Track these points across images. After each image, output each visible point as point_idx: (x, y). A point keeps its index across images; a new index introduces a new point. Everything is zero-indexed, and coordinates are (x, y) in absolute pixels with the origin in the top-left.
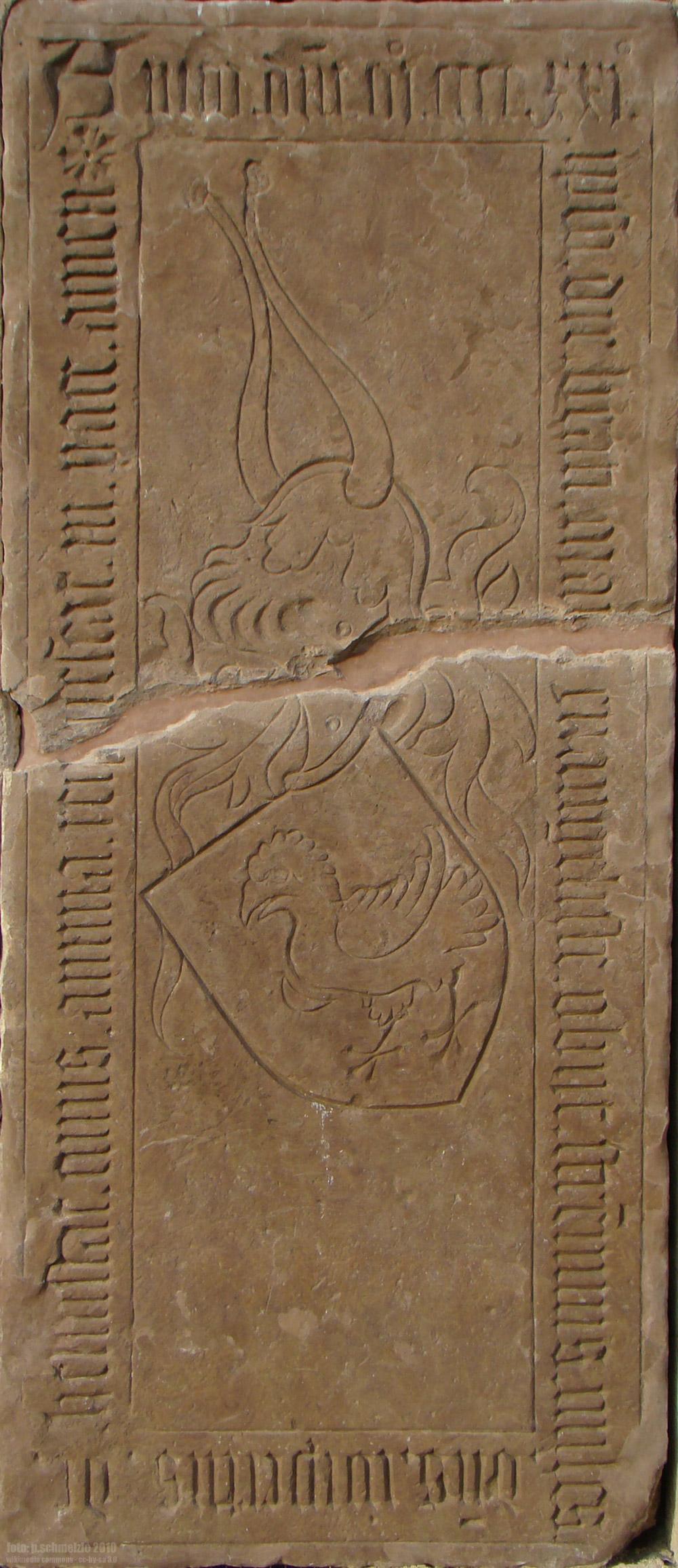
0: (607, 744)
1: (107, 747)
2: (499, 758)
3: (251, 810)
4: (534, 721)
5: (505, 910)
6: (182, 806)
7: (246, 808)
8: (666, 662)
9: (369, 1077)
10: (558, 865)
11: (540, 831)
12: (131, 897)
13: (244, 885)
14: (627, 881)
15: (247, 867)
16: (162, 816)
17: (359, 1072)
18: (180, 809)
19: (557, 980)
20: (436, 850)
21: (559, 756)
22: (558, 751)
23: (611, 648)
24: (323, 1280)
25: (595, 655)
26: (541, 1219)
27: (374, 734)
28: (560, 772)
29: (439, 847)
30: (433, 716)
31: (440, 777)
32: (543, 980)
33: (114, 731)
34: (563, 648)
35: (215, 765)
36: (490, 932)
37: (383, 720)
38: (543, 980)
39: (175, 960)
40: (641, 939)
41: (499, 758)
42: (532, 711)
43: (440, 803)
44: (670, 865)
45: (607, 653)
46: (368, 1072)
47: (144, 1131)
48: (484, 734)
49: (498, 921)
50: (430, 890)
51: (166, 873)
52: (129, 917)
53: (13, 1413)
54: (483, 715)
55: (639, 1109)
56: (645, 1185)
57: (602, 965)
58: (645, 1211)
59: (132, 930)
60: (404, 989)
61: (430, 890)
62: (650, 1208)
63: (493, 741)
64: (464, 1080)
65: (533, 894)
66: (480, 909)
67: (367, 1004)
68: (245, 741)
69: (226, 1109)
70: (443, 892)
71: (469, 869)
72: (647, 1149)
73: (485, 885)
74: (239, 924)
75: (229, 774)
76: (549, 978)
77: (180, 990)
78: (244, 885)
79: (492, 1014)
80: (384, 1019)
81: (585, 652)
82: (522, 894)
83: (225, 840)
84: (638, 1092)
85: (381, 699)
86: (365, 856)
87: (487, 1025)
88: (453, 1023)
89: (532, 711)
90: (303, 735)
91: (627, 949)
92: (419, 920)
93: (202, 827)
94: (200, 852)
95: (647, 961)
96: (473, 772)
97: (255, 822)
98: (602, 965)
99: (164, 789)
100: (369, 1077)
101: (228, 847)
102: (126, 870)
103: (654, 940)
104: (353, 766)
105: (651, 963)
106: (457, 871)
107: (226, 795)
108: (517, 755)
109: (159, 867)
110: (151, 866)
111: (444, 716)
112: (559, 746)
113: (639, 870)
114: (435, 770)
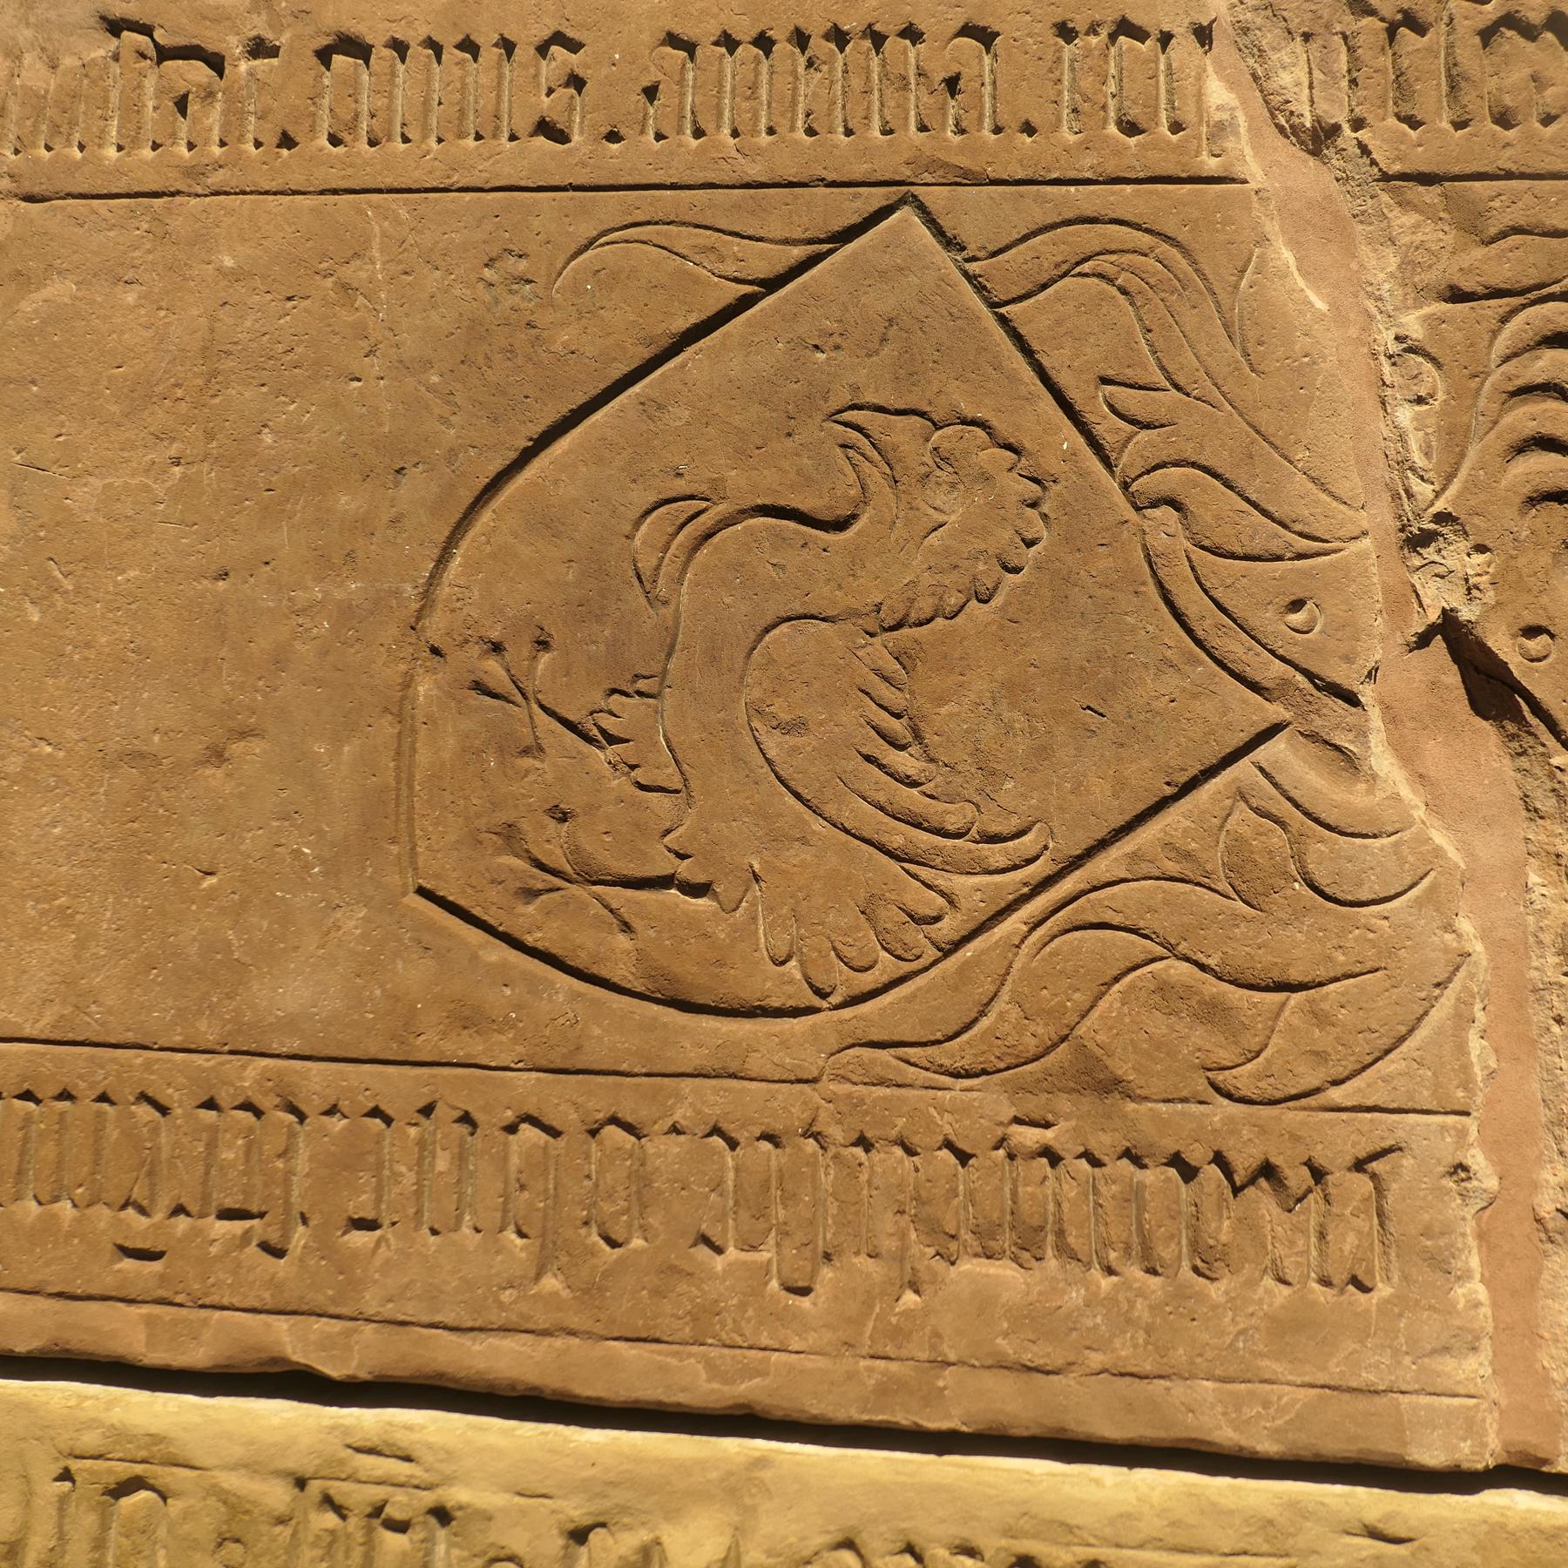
0: (1252, 1283)
1: (1241, 119)
2: (1213, 1013)
3: (1099, 430)
4: (1311, 1101)
5: (847, 1013)
6: (1111, 281)
7: (1108, 428)
8: (1466, 1447)
9: (480, 687)
10: (949, 1145)
11: (1033, 1105)
12: (906, 173)
13: (922, 414)
14: (908, 1314)
15: (964, 422)
16: (1090, 237)
17: (493, 669)
18: (1101, 276)
19: (434, 1232)
20: (996, 854)
21: (1219, 1159)
22: (1231, 1156)
23: (1495, 1305)
24: (68, 585)
25: (1475, 1262)
26: (147, 1066)
27: (1276, 711)
28: (1176, 1161)
29: (1002, 862)
30: (1323, 854)
31: (1172, 868)
32: (680, 1098)
33: (1281, 141)
34: (1492, 1183)
35: (1203, 349)
36: (799, 976)
37: (1313, 737)
38: (680, 1098)
39: (763, 270)
40: (765, 1340)
41: (1213, 1013)
42: (1336, 1095)
43: (1104, 865)
44: (945, 1425)
45: (1482, 1294)
46: (492, 685)
47: (403, 213)
48: (1276, 975)
49: (823, 995)
50: (900, 834)
51: (950, 243)
52: (858, 171)
53: (1421, 776)
54: (1322, 973)
55: (370, 1311)
56: (204, 1313)
57: (706, 1240)
58: (145, 1310)
59: (831, 177)
60: (673, 769)
61: (900, 834)
62: (149, 1321)
63: (1257, 996)
64: (462, 902)
65: (881, 1082)
66: (850, 953)
67: (642, 685)
68: (1264, 418)
69: (435, 379)
70: (895, 867)
71: (948, 928)
72: (282, 1324)
73: (907, 967)
74: (834, 404)
75: (1182, 381)
76: (681, 1115)
77: (696, 280)
78: (922, 414)
79: (604, 973)
80: (607, 722)
81: (1481, 1236)
82: (885, 1055)
83: (1028, 374)
84: (410, 1311)
85: (1362, 734)
86: (980, 686)
87: (581, 961)
88: (593, 879)
89: (1336, 1095)
90: (1275, 547)
91: (743, 1306)
92: (830, 810)
93: (1059, 323)
94: (1003, 321)
95: (714, 1353)
96: (1183, 948)
97: (1071, 438)
98: (706, 1240)
99: (1147, 239)
100: (480, 687)
101: (1013, 378)
102: (964, 162)
103: (763, 1374)
104: (1201, 663)
105: (710, 1365)
106: (941, 901)
107: (1130, 374)
108: (1225, 1056)
109: (972, 233)
110: (976, 215)
111: (1322, 880)
112: (1243, 1164)
113: (933, 1348)
114: (1188, 856)
